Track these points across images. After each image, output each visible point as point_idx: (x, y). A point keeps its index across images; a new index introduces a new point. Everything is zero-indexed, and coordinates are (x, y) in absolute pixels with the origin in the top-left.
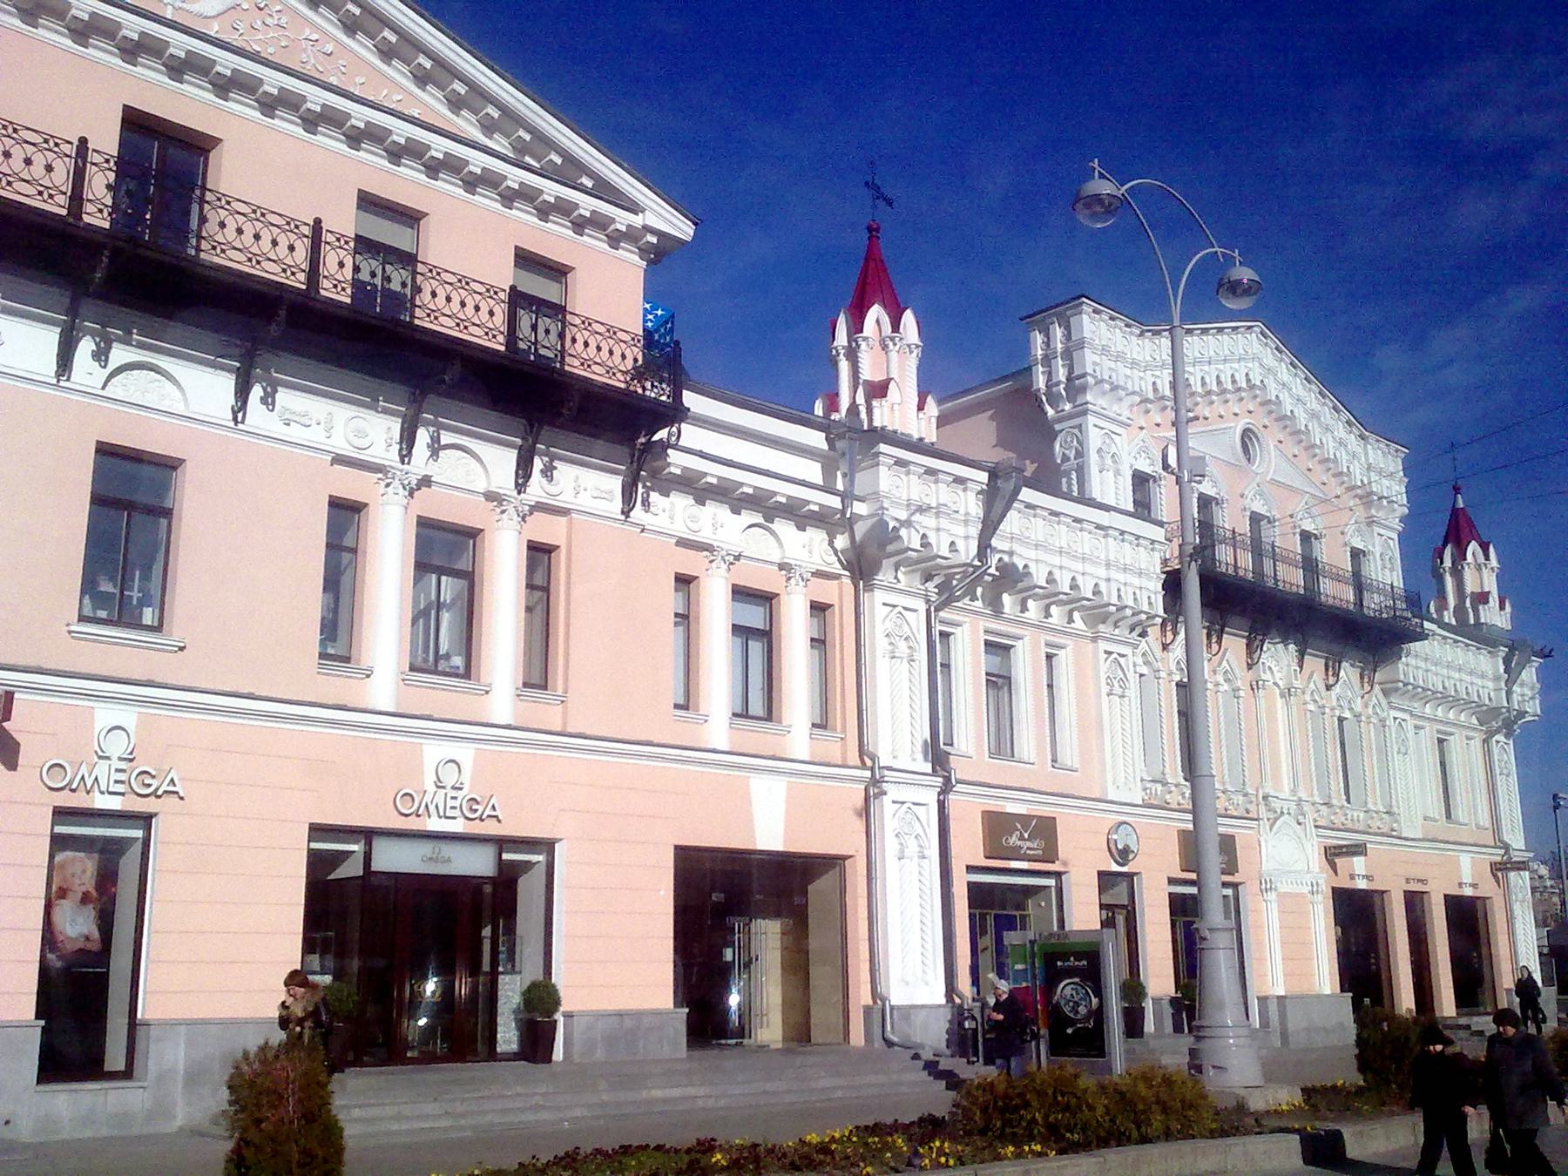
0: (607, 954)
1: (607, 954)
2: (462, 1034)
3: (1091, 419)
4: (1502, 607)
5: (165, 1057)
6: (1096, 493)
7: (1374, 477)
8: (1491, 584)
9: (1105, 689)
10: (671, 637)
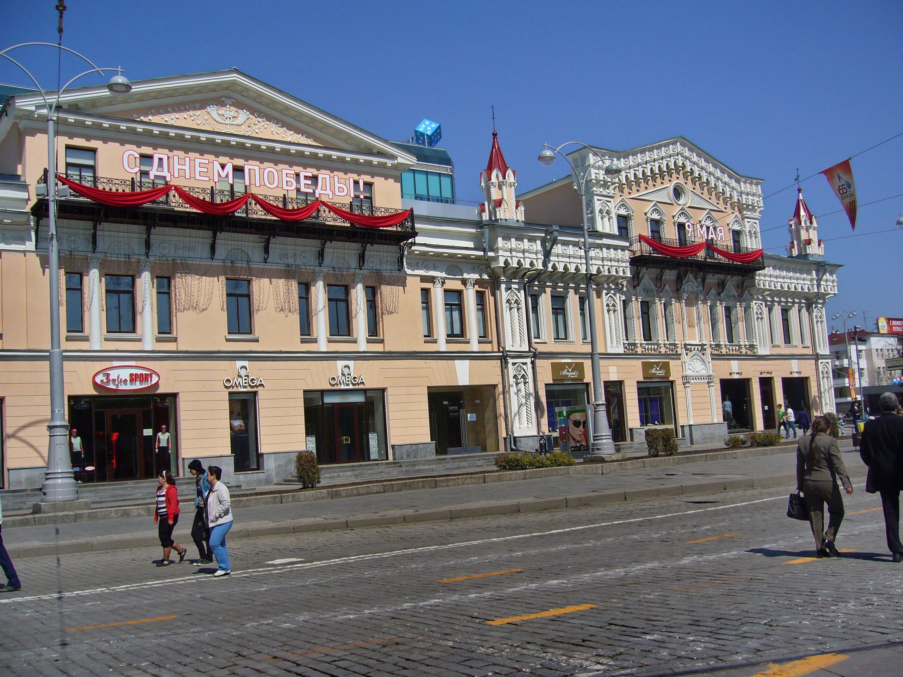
0: (408, 423)
1: (408, 423)
2: (359, 453)
3: (596, 198)
4: (819, 245)
5: (270, 464)
6: (599, 228)
7: (744, 196)
8: (814, 235)
9: (605, 308)
10: (421, 315)
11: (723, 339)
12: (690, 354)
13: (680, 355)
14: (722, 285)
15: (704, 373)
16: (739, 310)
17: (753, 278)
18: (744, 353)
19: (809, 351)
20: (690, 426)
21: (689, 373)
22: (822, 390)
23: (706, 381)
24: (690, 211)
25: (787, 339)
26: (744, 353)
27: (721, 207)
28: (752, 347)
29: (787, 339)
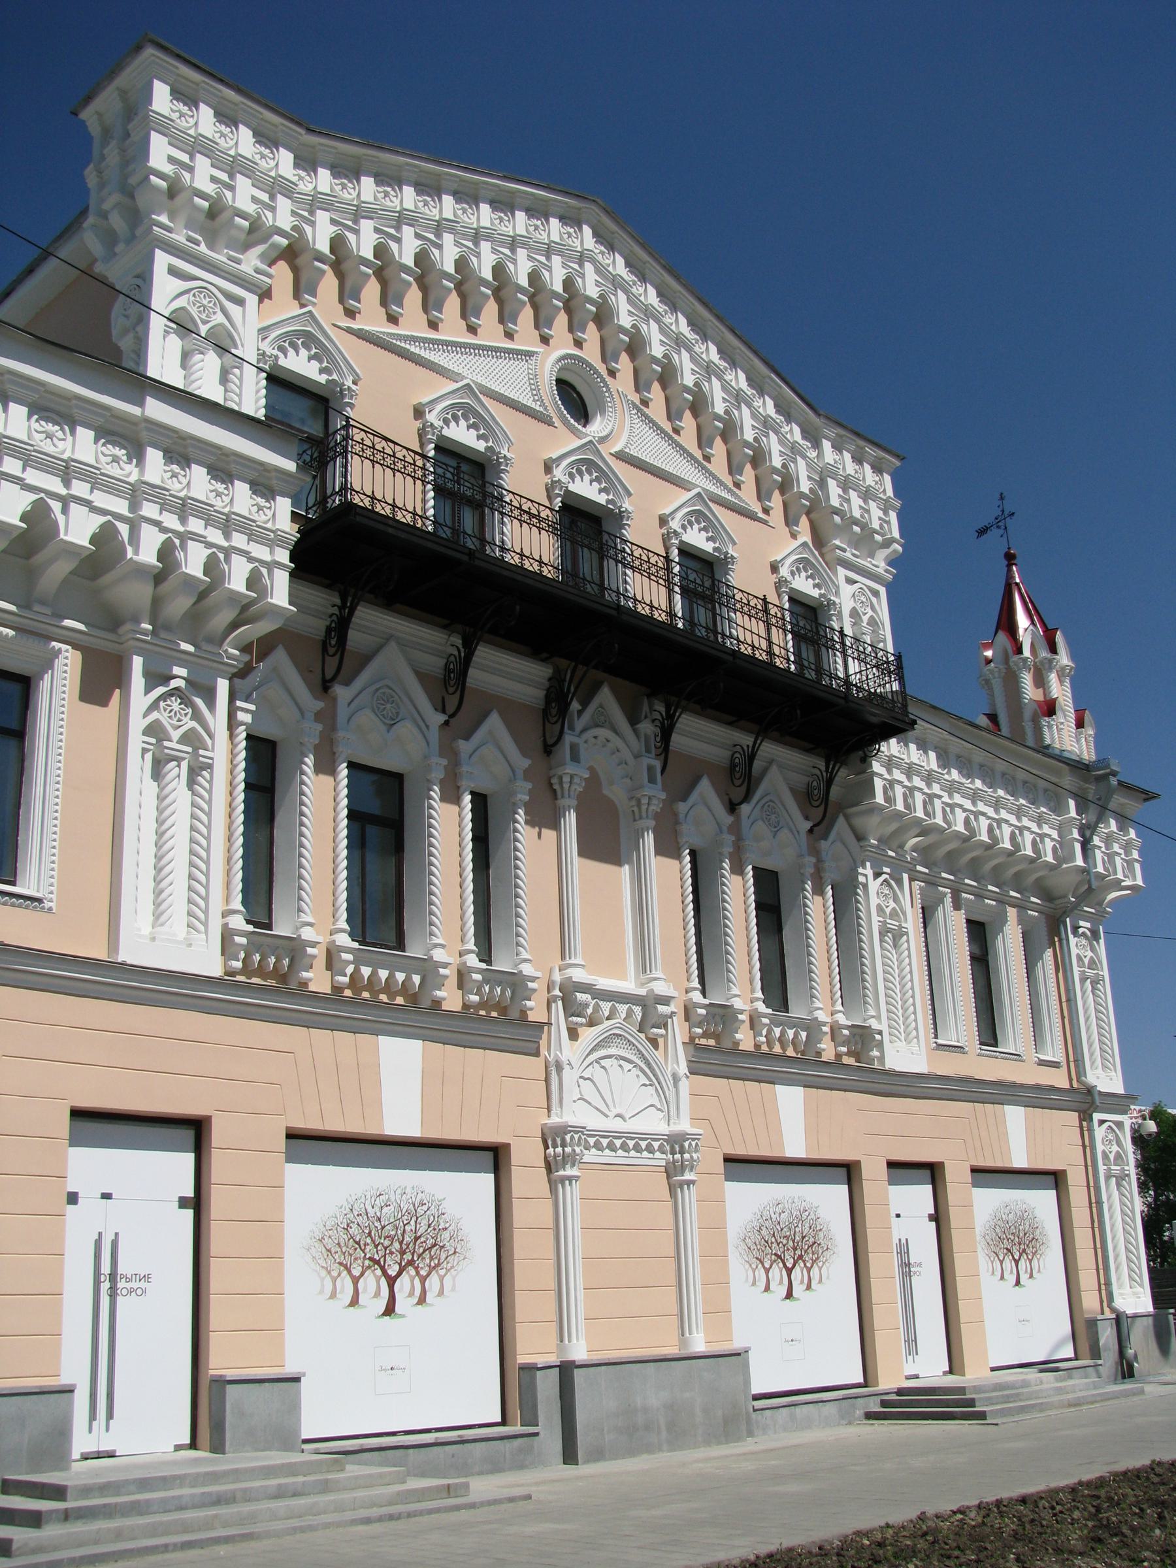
4: (1080, 724)
11: (743, 991)
12: (588, 1035)
13: (539, 1026)
14: (739, 781)
15: (655, 1124)
16: (817, 910)
17: (865, 760)
18: (828, 1054)
19: (1059, 1079)
20: (566, 1370)
21: (572, 1114)
22: (329, 492)
23: (660, 1159)
24: (622, 470)
25: (990, 1033)
26: (828, 1054)
27: (748, 496)
28: (862, 1039)
29: (990, 1033)
